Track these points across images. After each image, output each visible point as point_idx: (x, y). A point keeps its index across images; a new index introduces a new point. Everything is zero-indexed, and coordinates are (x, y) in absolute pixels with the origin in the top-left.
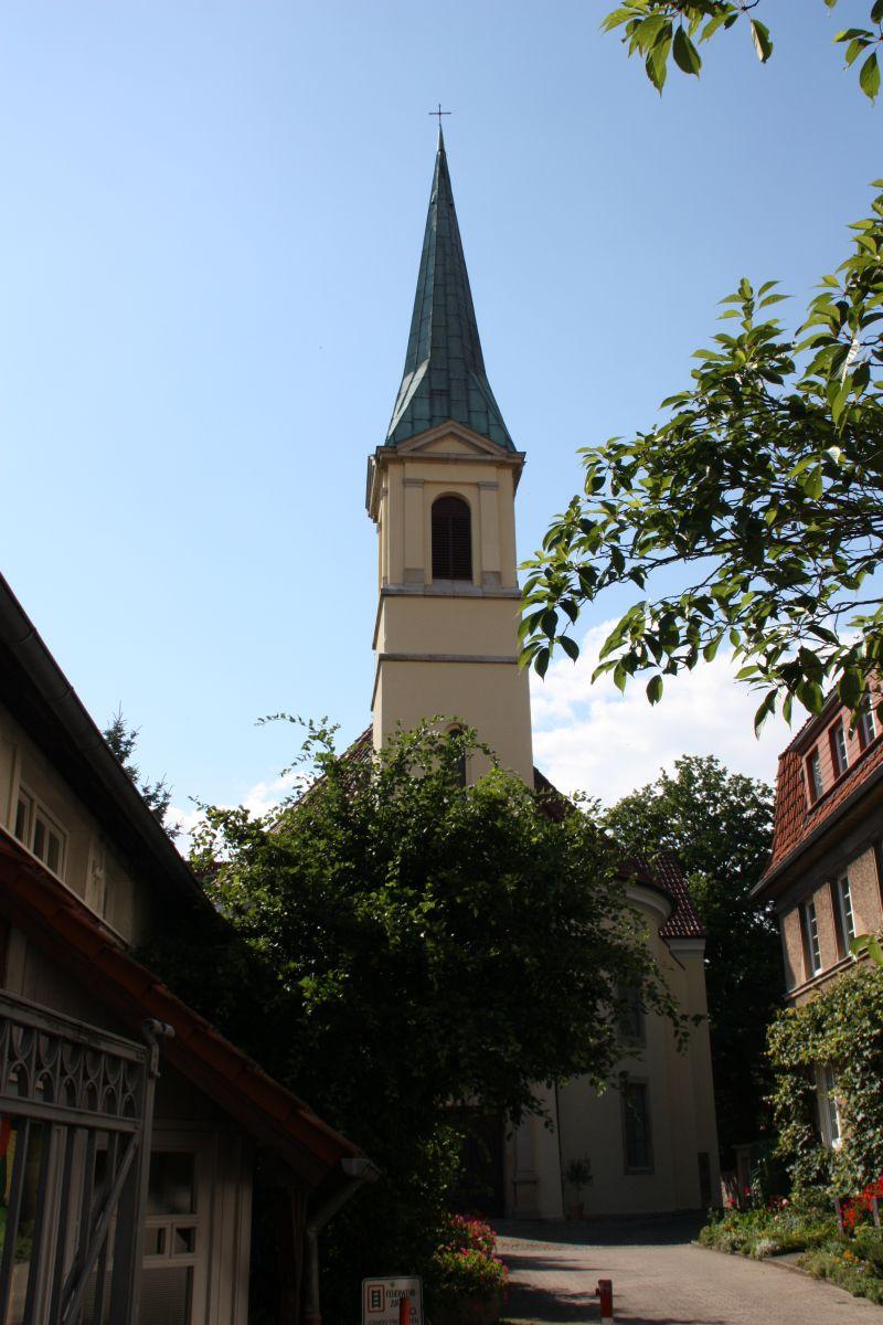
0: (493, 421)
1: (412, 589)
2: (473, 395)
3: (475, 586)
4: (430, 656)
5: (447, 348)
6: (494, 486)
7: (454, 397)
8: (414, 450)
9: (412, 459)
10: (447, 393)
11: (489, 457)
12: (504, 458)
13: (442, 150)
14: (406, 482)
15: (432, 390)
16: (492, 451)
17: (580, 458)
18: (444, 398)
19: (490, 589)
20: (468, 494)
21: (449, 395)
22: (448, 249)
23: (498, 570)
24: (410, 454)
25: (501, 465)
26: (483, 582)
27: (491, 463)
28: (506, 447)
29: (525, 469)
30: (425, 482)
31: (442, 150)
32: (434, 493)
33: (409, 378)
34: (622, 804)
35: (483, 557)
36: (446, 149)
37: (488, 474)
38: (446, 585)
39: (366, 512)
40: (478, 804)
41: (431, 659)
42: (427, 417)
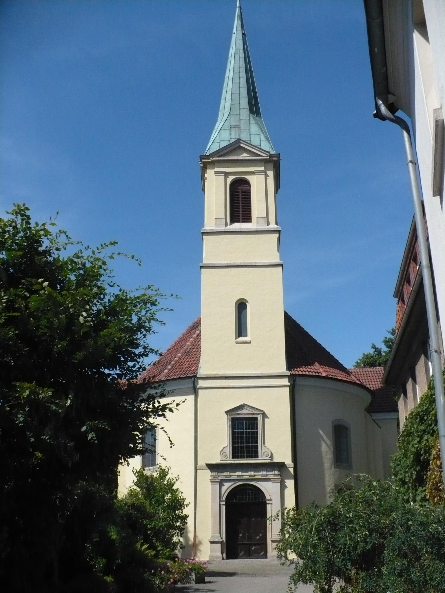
10: (239, 127)
20: (248, 177)
26: (258, 223)
32: (231, 179)
38: (237, 226)
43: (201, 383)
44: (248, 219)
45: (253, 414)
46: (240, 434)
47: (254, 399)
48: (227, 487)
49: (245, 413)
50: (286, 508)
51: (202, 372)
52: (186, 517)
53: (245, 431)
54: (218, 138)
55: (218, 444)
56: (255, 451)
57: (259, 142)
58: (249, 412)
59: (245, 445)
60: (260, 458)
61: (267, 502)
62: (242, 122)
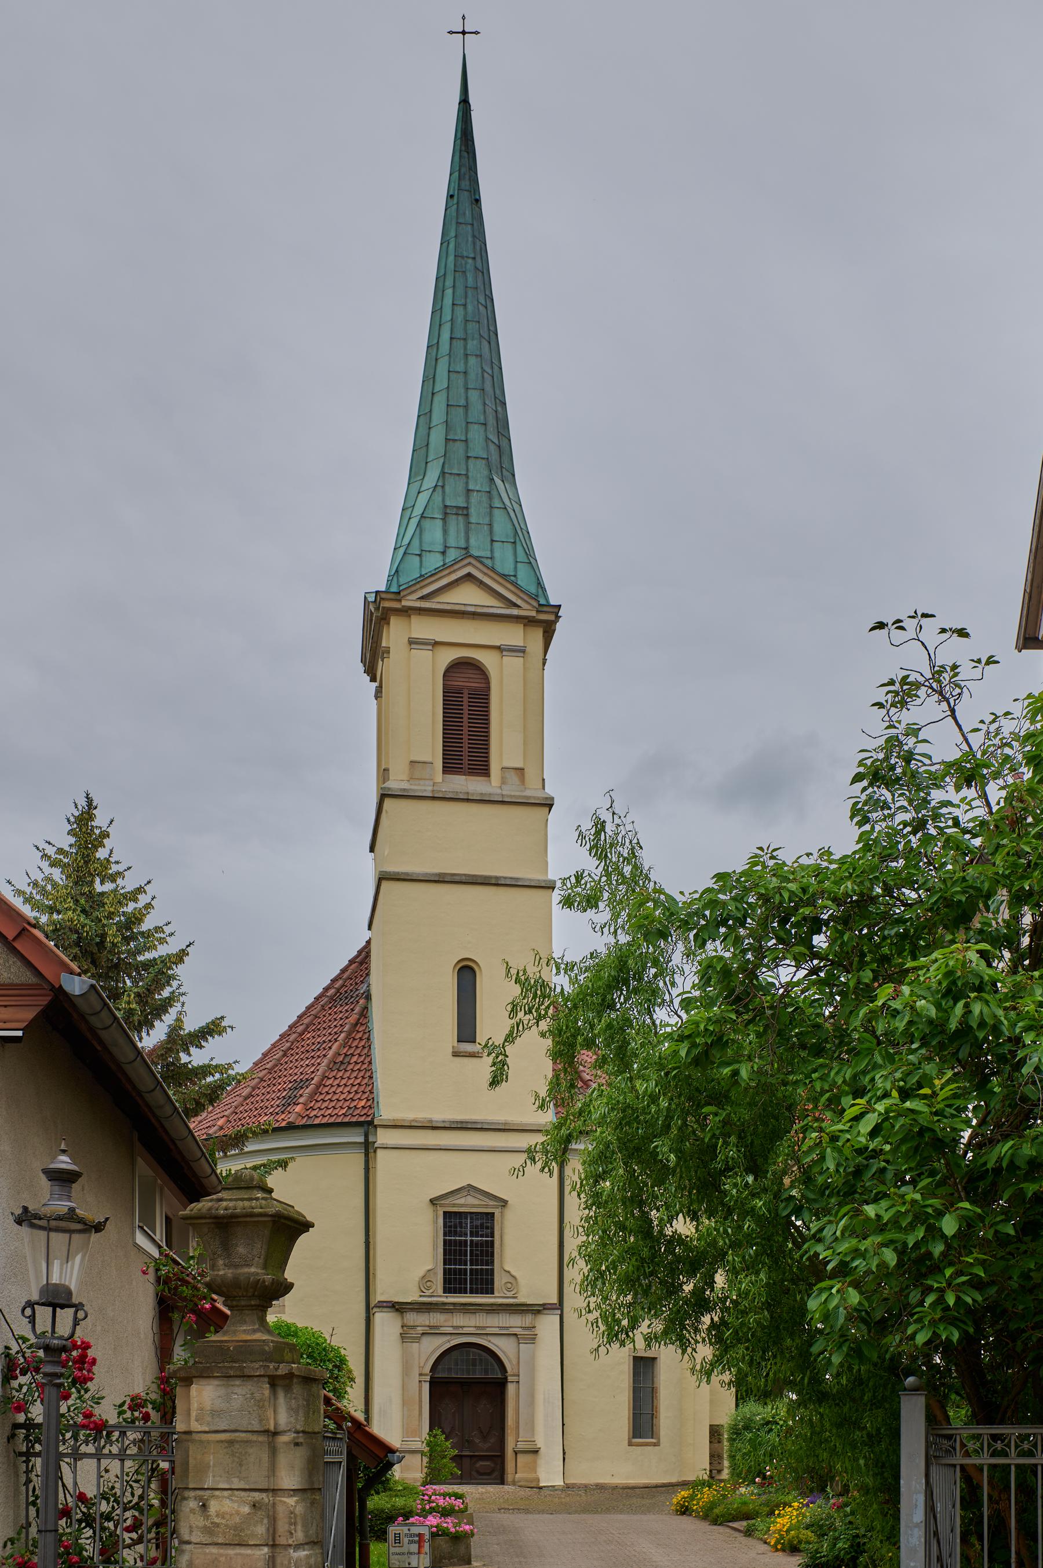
0: (521, 556)
1: (419, 788)
2: (498, 515)
3: (492, 785)
4: (440, 875)
5: (466, 441)
6: (521, 651)
7: (473, 519)
8: (422, 598)
9: (421, 611)
10: (464, 512)
11: (515, 612)
12: (533, 614)
13: (465, 102)
14: (412, 642)
15: (446, 507)
16: (519, 602)
17: (428, 1213)
18: (460, 518)
19: (512, 790)
20: (488, 660)
21: (467, 515)
22: (470, 280)
23: (520, 765)
24: (418, 604)
25: (529, 622)
26: (504, 781)
27: (517, 619)
28: (535, 598)
29: (559, 626)
30: (436, 644)
31: (465, 102)
32: (448, 656)
33: (415, 487)
34: (199, 1032)
35: (505, 747)
36: (472, 100)
37: (512, 635)
38: (461, 783)
39: (361, 668)
40: (858, 1519)
41: (440, 879)
42: (441, 548)
43: (383, 1137)
44: (481, 768)
45: (487, 1206)
46: (460, 1246)
47: (490, 1173)
48: (432, 1348)
49: (468, 1204)
50: (543, 1035)
51: (386, 1112)
52: (289, 1227)
53: (469, 1246)
54: (416, 542)
55: (413, 1258)
56: (487, 1279)
57: (512, 566)
58: (476, 1202)
59: (468, 1267)
60: (496, 1294)
61: (510, 1379)
62: (474, 498)
